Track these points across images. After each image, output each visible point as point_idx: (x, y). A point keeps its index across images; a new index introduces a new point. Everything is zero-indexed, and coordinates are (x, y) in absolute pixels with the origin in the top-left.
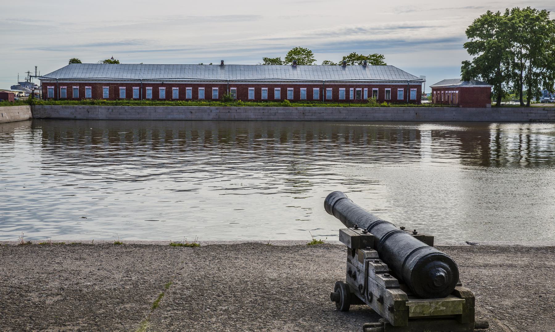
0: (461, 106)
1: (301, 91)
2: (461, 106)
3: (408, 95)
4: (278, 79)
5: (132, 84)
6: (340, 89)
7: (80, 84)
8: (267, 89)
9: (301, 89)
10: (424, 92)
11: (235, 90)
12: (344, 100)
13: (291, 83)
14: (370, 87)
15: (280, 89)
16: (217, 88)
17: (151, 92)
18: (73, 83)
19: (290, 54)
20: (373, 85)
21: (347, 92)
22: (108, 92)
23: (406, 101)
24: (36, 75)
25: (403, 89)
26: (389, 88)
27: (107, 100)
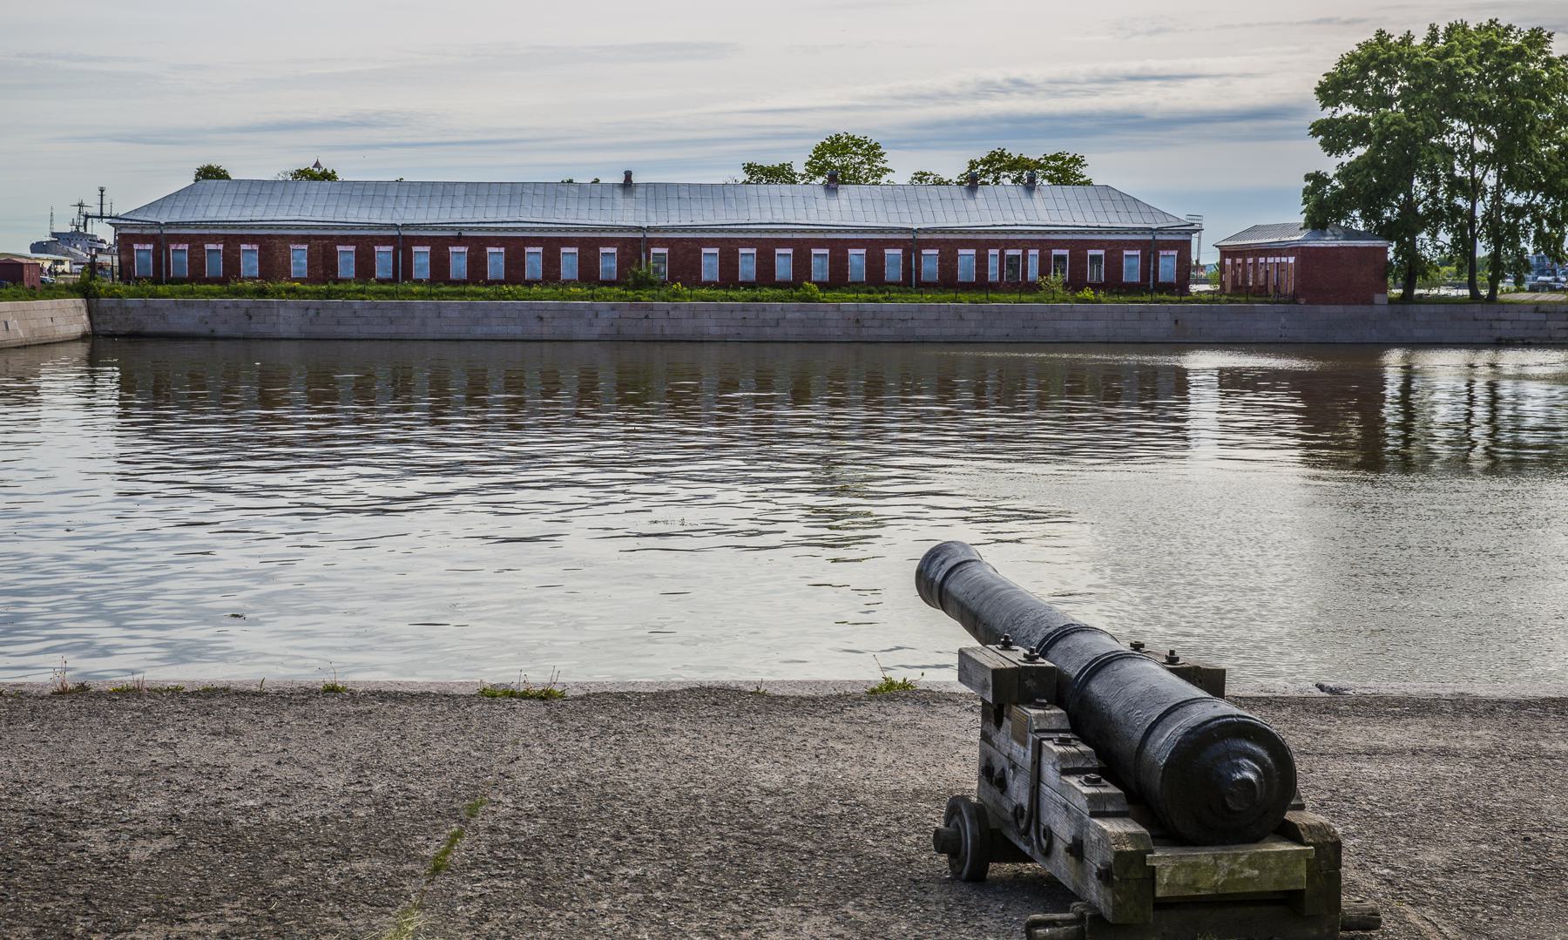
0: (1302, 301)
1: (851, 258)
2: (1302, 301)
3: (1152, 269)
4: (785, 224)
5: (372, 237)
6: (961, 252)
7: (226, 239)
8: (754, 251)
9: (851, 251)
10: (1197, 261)
11: (664, 254)
12: (972, 283)
13: (821, 236)
14: (1045, 245)
15: (790, 251)
16: (614, 250)
17: (427, 260)
18: (205, 235)
19: (820, 152)
20: (1053, 241)
21: (982, 261)
22: (305, 261)
23: (1148, 285)
24: (102, 213)
25: (1138, 252)
26: (1099, 249)
27: (303, 283)
